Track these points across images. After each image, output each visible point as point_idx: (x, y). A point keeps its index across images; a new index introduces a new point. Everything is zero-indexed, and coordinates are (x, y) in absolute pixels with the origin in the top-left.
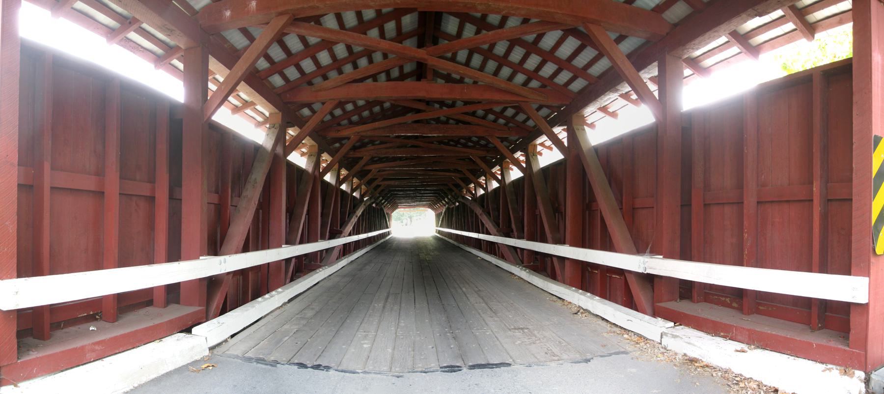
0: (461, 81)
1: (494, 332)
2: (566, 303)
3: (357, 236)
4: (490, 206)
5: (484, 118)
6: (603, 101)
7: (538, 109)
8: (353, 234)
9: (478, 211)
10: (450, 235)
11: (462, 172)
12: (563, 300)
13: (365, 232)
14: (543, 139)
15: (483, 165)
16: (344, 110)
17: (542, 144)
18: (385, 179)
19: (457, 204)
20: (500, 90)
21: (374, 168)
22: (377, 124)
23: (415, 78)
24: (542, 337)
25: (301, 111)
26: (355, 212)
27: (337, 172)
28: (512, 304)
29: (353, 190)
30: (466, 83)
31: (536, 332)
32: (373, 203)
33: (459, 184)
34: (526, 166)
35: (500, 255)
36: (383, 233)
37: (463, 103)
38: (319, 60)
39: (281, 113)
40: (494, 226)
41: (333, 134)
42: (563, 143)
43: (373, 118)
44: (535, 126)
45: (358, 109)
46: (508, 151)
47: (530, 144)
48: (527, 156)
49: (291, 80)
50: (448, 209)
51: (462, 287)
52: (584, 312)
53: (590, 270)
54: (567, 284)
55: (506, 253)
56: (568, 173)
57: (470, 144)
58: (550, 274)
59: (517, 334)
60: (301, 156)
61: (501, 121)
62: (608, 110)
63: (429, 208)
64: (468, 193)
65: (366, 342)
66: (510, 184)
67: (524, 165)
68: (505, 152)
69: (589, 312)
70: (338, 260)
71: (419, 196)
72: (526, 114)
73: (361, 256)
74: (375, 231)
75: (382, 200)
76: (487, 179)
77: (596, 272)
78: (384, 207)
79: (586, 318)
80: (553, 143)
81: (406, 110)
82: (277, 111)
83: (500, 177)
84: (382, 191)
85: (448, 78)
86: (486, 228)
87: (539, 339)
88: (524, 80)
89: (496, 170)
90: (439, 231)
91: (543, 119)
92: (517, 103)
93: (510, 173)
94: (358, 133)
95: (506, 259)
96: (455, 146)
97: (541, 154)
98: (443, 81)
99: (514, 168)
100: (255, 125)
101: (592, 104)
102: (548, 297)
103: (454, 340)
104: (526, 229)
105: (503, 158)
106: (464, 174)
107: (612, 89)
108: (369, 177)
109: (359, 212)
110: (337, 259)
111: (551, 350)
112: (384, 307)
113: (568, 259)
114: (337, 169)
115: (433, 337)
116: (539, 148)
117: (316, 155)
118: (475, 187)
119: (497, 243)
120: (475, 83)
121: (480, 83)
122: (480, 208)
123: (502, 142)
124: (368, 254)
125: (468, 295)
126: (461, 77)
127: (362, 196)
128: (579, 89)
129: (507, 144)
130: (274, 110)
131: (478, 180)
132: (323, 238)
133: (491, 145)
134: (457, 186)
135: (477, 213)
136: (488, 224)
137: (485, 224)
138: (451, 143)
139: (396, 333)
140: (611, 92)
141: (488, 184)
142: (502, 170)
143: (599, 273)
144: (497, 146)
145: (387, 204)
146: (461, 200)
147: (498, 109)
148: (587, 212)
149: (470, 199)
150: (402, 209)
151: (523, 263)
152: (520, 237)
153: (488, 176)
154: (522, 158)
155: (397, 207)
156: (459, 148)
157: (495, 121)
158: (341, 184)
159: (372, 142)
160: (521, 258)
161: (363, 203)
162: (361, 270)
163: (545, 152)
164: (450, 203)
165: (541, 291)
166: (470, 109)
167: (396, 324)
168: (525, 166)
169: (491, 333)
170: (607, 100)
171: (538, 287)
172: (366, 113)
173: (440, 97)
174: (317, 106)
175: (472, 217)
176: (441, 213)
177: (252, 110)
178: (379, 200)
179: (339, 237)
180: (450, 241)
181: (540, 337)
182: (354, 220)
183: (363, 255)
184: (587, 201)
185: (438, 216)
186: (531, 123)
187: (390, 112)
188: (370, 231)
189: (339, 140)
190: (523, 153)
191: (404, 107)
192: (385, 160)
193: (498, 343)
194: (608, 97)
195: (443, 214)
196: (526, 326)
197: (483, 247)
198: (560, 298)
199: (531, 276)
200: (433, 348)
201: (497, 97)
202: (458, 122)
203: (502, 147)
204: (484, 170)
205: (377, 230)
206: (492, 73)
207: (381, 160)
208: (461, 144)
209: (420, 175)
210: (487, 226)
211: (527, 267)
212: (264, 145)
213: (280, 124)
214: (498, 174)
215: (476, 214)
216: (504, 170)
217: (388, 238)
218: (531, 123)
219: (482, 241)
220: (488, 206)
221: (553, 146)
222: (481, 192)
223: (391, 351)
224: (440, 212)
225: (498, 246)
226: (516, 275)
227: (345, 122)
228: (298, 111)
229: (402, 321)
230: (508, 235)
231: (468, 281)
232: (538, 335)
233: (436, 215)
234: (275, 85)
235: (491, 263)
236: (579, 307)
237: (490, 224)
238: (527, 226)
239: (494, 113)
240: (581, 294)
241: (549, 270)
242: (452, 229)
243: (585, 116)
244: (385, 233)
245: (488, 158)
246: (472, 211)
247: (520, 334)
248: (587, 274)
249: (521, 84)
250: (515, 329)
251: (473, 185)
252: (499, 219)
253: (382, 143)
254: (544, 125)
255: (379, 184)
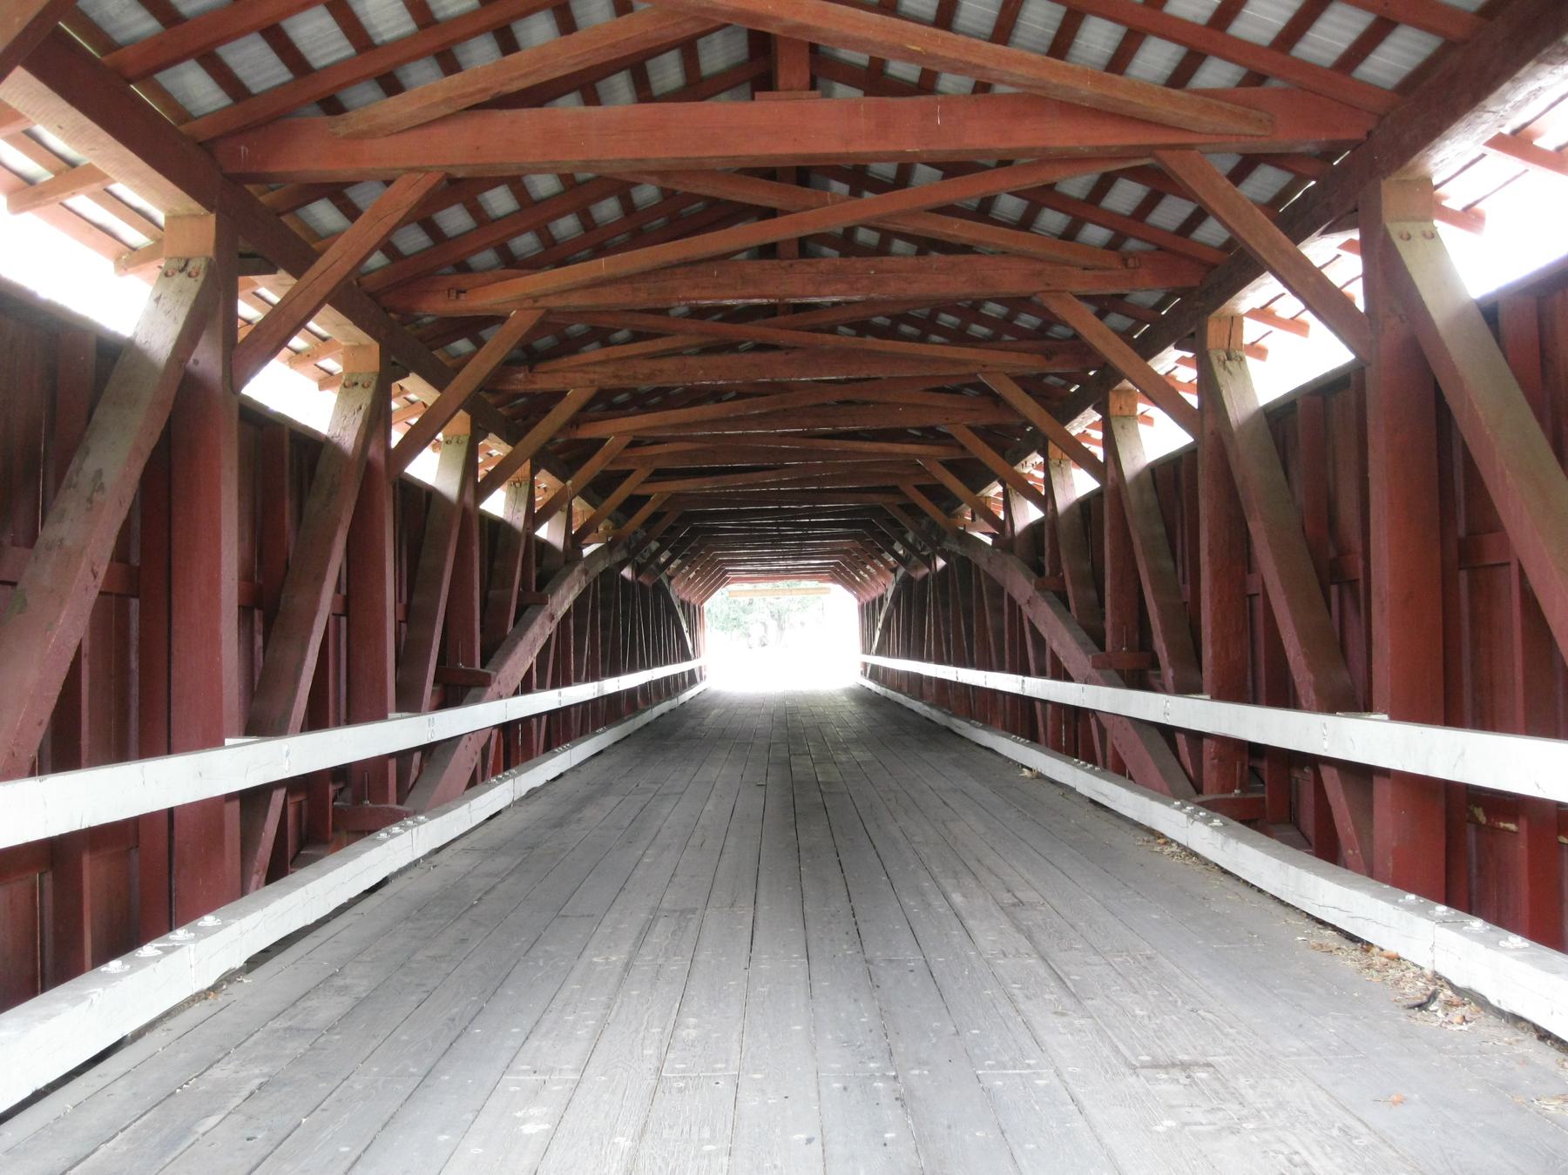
0: (926, 84)
1: (1066, 1077)
2: (1378, 961)
3: (556, 692)
4: (1065, 566)
5: (1025, 223)
6: (1508, 106)
7: (1238, 175)
8: (542, 686)
9: (1020, 586)
10: (916, 684)
11: (952, 437)
12: (1367, 946)
13: (593, 676)
14: (1264, 290)
15: (1029, 408)
16: (476, 211)
17: (1263, 313)
18: (660, 475)
19: (941, 563)
20: (1071, 109)
21: (615, 430)
22: (603, 266)
23: (747, 87)
24: (1270, 1103)
25: (301, 212)
26: (543, 602)
27: (464, 448)
28: (1149, 958)
29: (535, 519)
30: (941, 93)
31: (1242, 1083)
32: (622, 565)
33: (942, 486)
34: (1201, 403)
35: (1109, 759)
36: (666, 679)
37: (939, 173)
38: (364, 20)
39: (212, 217)
40: (1082, 645)
41: (437, 305)
42: (1347, 302)
43: (597, 243)
44: (1229, 245)
45: (532, 211)
46: (1128, 350)
47: (1214, 315)
48: (1203, 364)
49: (255, 90)
50: (906, 586)
51: (949, 889)
52: (1456, 999)
53: (1483, 819)
54: (1383, 880)
55: (1134, 751)
56: (1371, 422)
57: (978, 330)
58: (1311, 832)
59: (1164, 1087)
60: (321, 388)
61: (1095, 234)
62: (1537, 143)
63: (834, 580)
64: (980, 521)
65: (534, 1111)
66: (1138, 477)
67: (1193, 400)
68: (1116, 352)
69: (1482, 1003)
70: (473, 789)
71: (791, 538)
72: (1193, 201)
73: (572, 770)
74: (633, 669)
75: (659, 552)
76: (1052, 462)
77: (1512, 827)
78: (670, 578)
79: (1465, 1027)
80: (1309, 306)
81: (723, 214)
82: (195, 206)
83: (1099, 453)
84: (656, 517)
85: (874, 79)
86: (1053, 653)
87: (1258, 1115)
88: (1174, 65)
89: (1086, 425)
90: (875, 669)
91: (1258, 211)
92: (1150, 155)
93: (1137, 435)
94: (535, 299)
95: (1131, 778)
96: (922, 339)
97: (1259, 352)
98: (857, 93)
99: (1154, 412)
100: (117, 260)
101: (1460, 126)
102: (1303, 935)
103: (900, 1111)
104: (1208, 653)
105: (1110, 376)
106: (962, 447)
107: (1545, 51)
108: (594, 466)
109: (563, 600)
110: (472, 782)
111: (1306, 1164)
112: (628, 967)
113: (1385, 773)
114: (465, 439)
115: (814, 1095)
116: (1252, 331)
117: (373, 384)
118: (1005, 494)
119: (1094, 712)
120: (982, 88)
121: (1000, 89)
122: (1029, 580)
123: (1101, 315)
124: (604, 761)
125: (971, 923)
126: (924, 71)
127: (575, 541)
128: (1404, 74)
129: (1127, 323)
130: (186, 204)
131: (1018, 468)
132: (409, 703)
133: (1058, 331)
134: (939, 494)
135: (1016, 595)
136: (1062, 639)
137: (1046, 636)
138: (906, 329)
139: (659, 1070)
140: (1540, 61)
141: (1056, 480)
142: (1106, 426)
143: (1524, 836)
144: (1084, 332)
145: (680, 567)
146: (956, 548)
147: (1076, 185)
148: (1463, 574)
149: (988, 540)
150: (747, 586)
151: (1199, 791)
152: (1186, 687)
153: (1051, 447)
154: (1188, 374)
155: (719, 580)
156: (936, 347)
157: (1069, 235)
158: (484, 489)
159: (602, 336)
160: (1191, 772)
161: (580, 567)
162: (560, 823)
163: (1278, 341)
164: (914, 558)
165: (1272, 906)
166: (966, 191)
167: (662, 1033)
168: (1196, 406)
169: (1056, 1082)
170: (1527, 101)
171: (1260, 891)
172: (567, 226)
173: (843, 150)
174: (362, 196)
175: (998, 610)
176: (881, 599)
177: (95, 197)
178: (647, 555)
179: (477, 700)
180: (917, 706)
181: (1259, 1106)
182: (540, 631)
183: (580, 765)
184: (1462, 531)
185: (869, 611)
186: (1211, 233)
187: (660, 222)
188: (615, 672)
189: (474, 326)
190: (1189, 355)
191: (713, 202)
192: (653, 401)
193: (1079, 1123)
194: (1531, 86)
195: (886, 605)
196: (1205, 1054)
197: (1041, 729)
198: (1352, 938)
199: (1232, 842)
200: (809, 1141)
201: (1062, 135)
202: (926, 245)
203: (1101, 334)
204: (1036, 431)
205: (643, 667)
206: (1045, 50)
207: (640, 402)
208: (942, 331)
209: (791, 453)
210: (1055, 646)
211: (1213, 807)
212: (140, 340)
213: (209, 261)
214: (1094, 442)
215: (1012, 601)
216: (1115, 425)
217: (687, 695)
218: (1211, 233)
219: (1038, 705)
220: (1057, 568)
221: (1308, 317)
222: (1028, 514)
223: (629, 1144)
224: (875, 594)
225: (1100, 725)
226: (1169, 842)
227: (487, 258)
228: (292, 210)
229: (692, 1021)
230: (1139, 679)
231: (972, 864)
232: (1250, 1095)
233: (861, 608)
234: (190, 108)
235: (1072, 790)
236: (1437, 977)
237: (1067, 637)
238: (1213, 643)
239: (1062, 203)
240: (1443, 922)
241: (1308, 818)
242: (920, 658)
243: (1435, 181)
244: (675, 677)
245: (1051, 380)
246: (998, 590)
247: (1173, 1088)
248: (1472, 836)
249: (1162, 81)
250: (1155, 1065)
251: (999, 489)
252: (1103, 618)
253: (637, 337)
254: (1264, 235)
255: (639, 492)
